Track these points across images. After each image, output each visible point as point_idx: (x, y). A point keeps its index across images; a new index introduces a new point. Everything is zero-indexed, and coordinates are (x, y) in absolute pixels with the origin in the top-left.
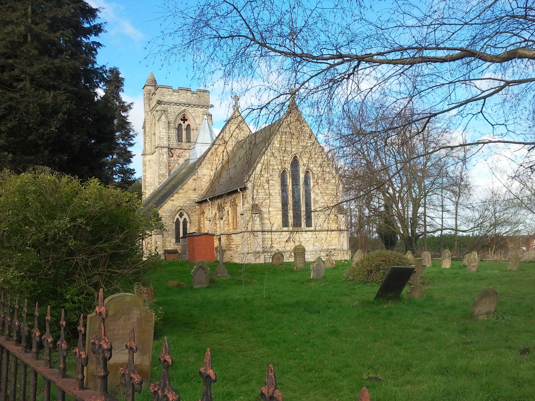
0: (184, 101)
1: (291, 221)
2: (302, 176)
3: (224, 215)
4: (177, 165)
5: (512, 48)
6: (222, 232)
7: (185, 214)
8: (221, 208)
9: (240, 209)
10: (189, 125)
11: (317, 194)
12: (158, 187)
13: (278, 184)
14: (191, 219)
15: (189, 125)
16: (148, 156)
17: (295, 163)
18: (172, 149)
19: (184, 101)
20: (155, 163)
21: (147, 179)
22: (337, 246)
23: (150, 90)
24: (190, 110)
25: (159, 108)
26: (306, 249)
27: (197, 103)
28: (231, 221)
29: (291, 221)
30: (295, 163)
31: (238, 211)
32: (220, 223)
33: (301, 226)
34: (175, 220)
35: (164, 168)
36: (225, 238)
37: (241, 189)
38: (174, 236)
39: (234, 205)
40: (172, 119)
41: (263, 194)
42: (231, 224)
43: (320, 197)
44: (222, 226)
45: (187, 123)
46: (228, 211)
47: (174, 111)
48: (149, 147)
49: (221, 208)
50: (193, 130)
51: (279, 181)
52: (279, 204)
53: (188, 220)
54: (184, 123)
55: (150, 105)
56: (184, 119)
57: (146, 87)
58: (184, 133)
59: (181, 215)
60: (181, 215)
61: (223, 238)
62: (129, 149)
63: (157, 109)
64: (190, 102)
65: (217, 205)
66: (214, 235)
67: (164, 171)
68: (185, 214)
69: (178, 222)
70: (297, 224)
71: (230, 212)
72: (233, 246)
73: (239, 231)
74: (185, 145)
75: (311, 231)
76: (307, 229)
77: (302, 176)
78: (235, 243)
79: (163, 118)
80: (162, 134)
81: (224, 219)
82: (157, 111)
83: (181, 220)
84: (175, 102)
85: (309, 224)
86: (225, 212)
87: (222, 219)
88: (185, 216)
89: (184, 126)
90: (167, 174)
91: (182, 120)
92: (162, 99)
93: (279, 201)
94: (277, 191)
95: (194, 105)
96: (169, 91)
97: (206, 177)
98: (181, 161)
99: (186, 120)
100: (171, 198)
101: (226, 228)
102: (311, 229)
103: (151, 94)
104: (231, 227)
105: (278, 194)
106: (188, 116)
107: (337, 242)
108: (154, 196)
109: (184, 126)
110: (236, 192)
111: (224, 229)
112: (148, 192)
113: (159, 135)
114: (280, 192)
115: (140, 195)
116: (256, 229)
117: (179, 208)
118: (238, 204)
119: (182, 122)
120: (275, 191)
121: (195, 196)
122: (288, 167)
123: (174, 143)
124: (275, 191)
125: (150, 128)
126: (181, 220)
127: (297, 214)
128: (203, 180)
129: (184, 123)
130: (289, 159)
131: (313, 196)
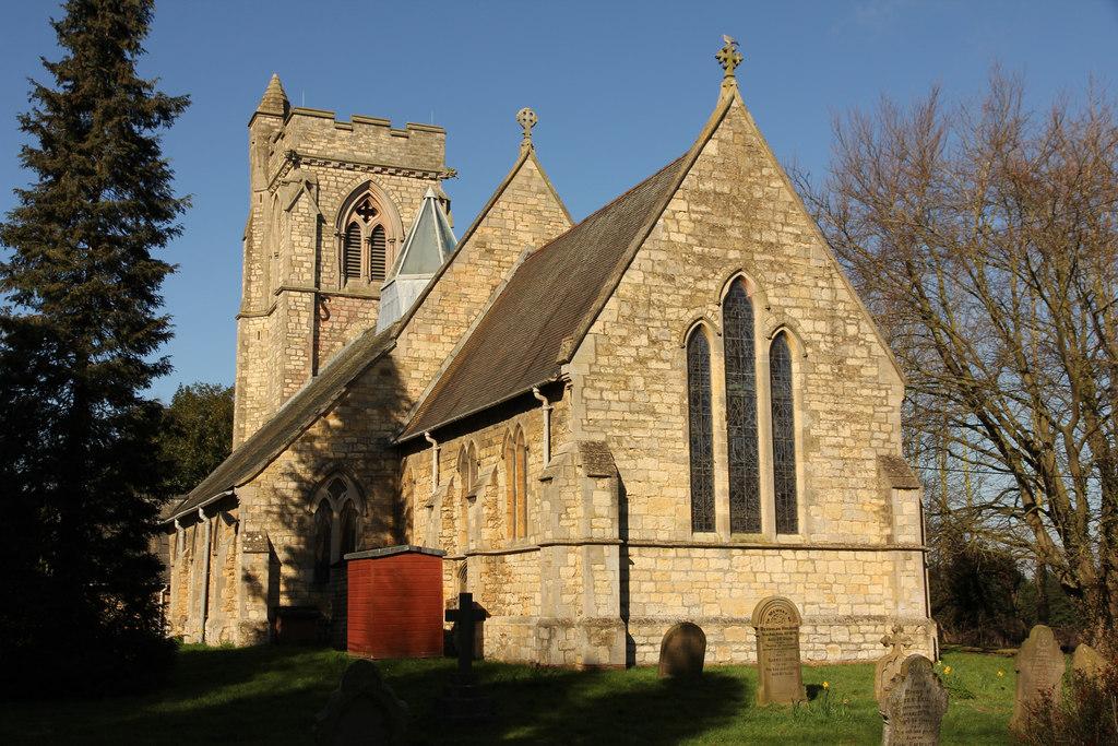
0: (368, 156)
1: (722, 509)
2: (761, 349)
4: (340, 344)
6: (472, 547)
8: (467, 463)
9: (538, 463)
10: (379, 228)
11: (814, 414)
12: (280, 409)
13: (679, 373)
15: (379, 228)
16: (256, 320)
17: (736, 303)
18: (327, 296)
19: (368, 156)
20: (275, 340)
21: (249, 390)
22: (890, 604)
23: (271, 129)
25: (293, 174)
26: (805, 612)
27: (405, 165)
28: (503, 506)
29: (722, 509)
30: (736, 303)
31: (531, 470)
32: (465, 514)
33: (757, 528)
35: (300, 353)
36: (483, 567)
37: (544, 390)
39: (519, 450)
40: (330, 207)
41: (624, 406)
42: (505, 518)
43: (824, 425)
44: (473, 523)
46: (495, 472)
47: (337, 185)
48: (259, 295)
49: (467, 463)
50: (393, 241)
51: (681, 360)
52: (680, 445)
54: (366, 220)
55: (267, 172)
56: (368, 212)
57: (259, 118)
58: (365, 248)
61: (476, 567)
62: (155, 252)
63: (289, 177)
64: (383, 160)
65: (455, 455)
66: (440, 556)
67: (300, 362)
70: (745, 519)
71: (502, 478)
72: (508, 598)
73: (533, 542)
74: (361, 283)
76: (785, 539)
77: (761, 349)
78: (516, 586)
79: (304, 203)
80: (297, 250)
81: (480, 499)
82: (285, 183)
84: (342, 157)
86: (484, 471)
87: (472, 498)
89: (365, 231)
90: (309, 371)
91: (360, 212)
92: (303, 148)
93: (680, 434)
94: (675, 399)
96: (324, 125)
97: (423, 367)
98: (354, 334)
99: (373, 212)
101: (487, 533)
103: (273, 139)
104: (504, 530)
105: (676, 409)
107: (888, 593)
109: (365, 231)
110: (525, 402)
111: (479, 534)
113: (288, 252)
114: (686, 402)
118: (534, 446)
123: (331, 278)
125: (265, 238)
127: (746, 484)
129: (366, 220)
131: (799, 420)
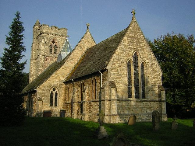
2: (140, 64)
3: (85, 89)
5: (134, 54)
7: (57, 89)
14: (60, 92)
17: (136, 57)
24: (57, 37)
30: (136, 57)
34: (50, 93)
35: (42, 66)
38: (49, 102)
45: (55, 44)
53: (58, 93)
54: (53, 44)
56: (54, 42)
59: (54, 90)
60: (54, 90)
68: (57, 89)
69: (52, 93)
75: (145, 101)
76: (143, 99)
77: (140, 64)
83: (54, 93)
85: (144, 97)
88: (57, 90)
89: (53, 45)
91: (52, 42)
93: (126, 80)
95: (59, 35)
100: (49, 79)
102: (145, 99)
106: (56, 41)
108: (33, 82)
109: (53, 45)
112: (31, 80)
115: (28, 82)
116: (113, 98)
117: (53, 85)
119: (52, 43)
120: (124, 73)
121: (63, 78)
122: (132, 58)
124: (124, 73)
126: (54, 93)
128: (68, 69)
129: (53, 44)
130: (132, 53)
